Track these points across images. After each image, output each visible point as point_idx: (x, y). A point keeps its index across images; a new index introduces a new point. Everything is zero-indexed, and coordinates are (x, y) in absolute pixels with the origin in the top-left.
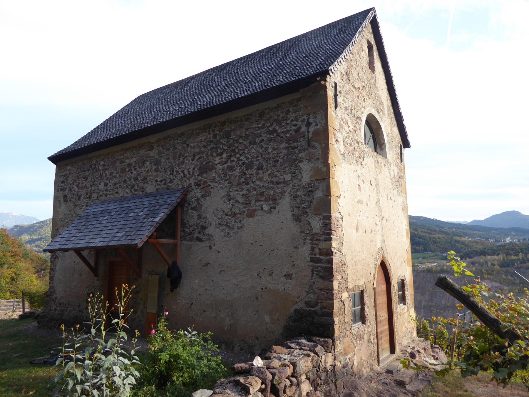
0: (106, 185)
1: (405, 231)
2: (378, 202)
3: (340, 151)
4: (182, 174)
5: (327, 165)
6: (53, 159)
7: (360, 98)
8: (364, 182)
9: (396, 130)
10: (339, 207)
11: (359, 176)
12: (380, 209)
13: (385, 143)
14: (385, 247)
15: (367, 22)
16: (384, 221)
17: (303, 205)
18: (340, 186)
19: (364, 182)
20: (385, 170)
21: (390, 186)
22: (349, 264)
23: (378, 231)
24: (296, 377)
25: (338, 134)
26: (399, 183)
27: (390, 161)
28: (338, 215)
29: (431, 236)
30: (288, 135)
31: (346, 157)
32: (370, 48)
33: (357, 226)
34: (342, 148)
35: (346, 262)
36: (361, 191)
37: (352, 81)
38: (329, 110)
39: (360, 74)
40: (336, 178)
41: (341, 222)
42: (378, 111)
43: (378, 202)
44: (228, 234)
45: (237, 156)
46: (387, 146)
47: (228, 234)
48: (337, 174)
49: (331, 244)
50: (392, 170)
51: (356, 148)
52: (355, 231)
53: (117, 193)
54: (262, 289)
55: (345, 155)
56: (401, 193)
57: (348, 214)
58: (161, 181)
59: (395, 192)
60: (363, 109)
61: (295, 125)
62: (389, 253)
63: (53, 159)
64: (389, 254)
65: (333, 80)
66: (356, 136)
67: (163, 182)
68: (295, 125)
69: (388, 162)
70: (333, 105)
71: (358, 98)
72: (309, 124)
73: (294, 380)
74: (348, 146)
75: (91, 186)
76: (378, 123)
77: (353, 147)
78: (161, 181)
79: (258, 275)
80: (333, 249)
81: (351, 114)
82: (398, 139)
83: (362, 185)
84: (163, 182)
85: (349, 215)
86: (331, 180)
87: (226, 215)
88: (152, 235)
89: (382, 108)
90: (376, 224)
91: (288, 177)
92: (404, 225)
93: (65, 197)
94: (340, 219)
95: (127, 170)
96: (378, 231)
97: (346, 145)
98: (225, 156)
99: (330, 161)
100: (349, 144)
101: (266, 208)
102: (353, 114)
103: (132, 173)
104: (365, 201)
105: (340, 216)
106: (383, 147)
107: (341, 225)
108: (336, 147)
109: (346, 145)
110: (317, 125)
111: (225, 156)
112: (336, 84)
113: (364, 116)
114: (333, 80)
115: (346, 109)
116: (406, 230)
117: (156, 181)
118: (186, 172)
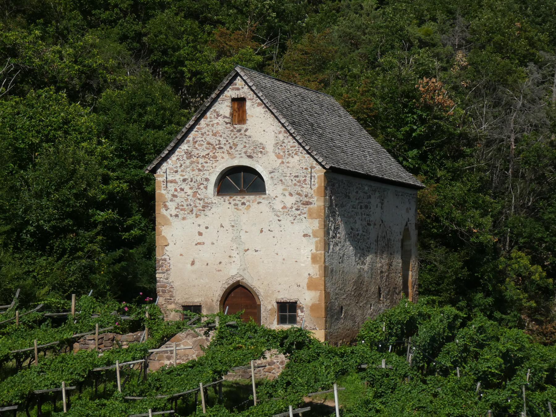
3: (171, 215)
10: (167, 252)
25: (169, 204)
40: (163, 234)
52: (189, 265)
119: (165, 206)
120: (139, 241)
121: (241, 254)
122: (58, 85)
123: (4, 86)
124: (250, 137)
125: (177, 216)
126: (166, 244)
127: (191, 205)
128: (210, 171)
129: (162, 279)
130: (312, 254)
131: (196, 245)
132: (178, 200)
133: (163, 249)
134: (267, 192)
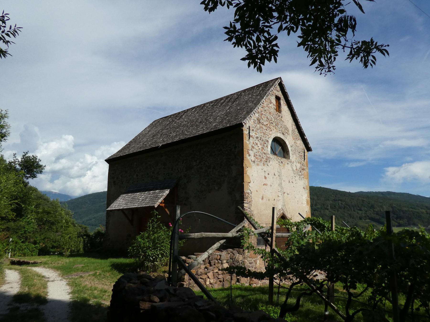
0: (137, 175)
1: (306, 201)
2: (280, 185)
3: (252, 160)
4: (177, 171)
5: (243, 168)
6: (108, 161)
7: (268, 130)
8: (268, 174)
9: (300, 142)
10: (250, 188)
11: (265, 171)
12: (282, 188)
13: (289, 151)
14: (285, 209)
15: (277, 83)
16: (286, 194)
17: (232, 187)
18: (250, 177)
19: (268, 174)
20: (288, 167)
21: (293, 175)
22: (256, 215)
23: (280, 200)
24: (221, 261)
25: (250, 152)
26: (301, 173)
27: (293, 161)
28: (249, 191)
29: (414, 210)
30: (227, 152)
31: (256, 162)
32: (278, 99)
33: (263, 197)
34: (253, 158)
35: (253, 214)
36: (266, 179)
37: (262, 122)
38: (245, 141)
39: (268, 117)
40: (248, 174)
41: (251, 195)
42: (283, 134)
43: (280, 185)
44: (199, 201)
45: (204, 162)
46: (291, 153)
47: (199, 201)
48: (248, 171)
49: (244, 205)
50: (294, 166)
51: (264, 157)
52: (261, 199)
53: (143, 180)
54: (214, 228)
55: (255, 162)
56: (303, 178)
57: (256, 191)
58: (167, 174)
59: (297, 178)
60: (270, 136)
61: (230, 147)
62: (289, 212)
63: (108, 161)
64: (288, 213)
65: (248, 125)
66: (264, 150)
67: (168, 175)
68: (230, 147)
69: (291, 162)
70: (248, 138)
71: (267, 130)
72: (235, 147)
73: (220, 261)
74: (258, 157)
75: (129, 176)
76: (283, 140)
77: (262, 157)
78: (167, 174)
79: (212, 221)
80: (245, 207)
81: (260, 140)
82: (302, 146)
83: (267, 176)
84: (168, 175)
85: (257, 191)
86: (245, 175)
87: (198, 192)
88: (162, 202)
89: (287, 131)
90: (278, 196)
91: (226, 173)
92: (305, 197)
93: (114, 182)
94: (250, 193)
95: (149, 167)
96: (280, 200)
97: (256, 156)
98: (198, 161)
99: (244, 165)
100: (258, 156)
101: (216, 188)
102: (262, 139)
103: (151, 169)
104: (269, 184)
105: (250, 192)
106: (288, 153)
107: (251, 196)
108: (249, 158)
109: (256, 156)
110: (239, 148)
111: (198, 161)
112: (249, 127)
113: (270, 139)
114: (248, 125)
115: (257, 138)
116: (307, 200)
117: (164, 174)
118: (179, 169)
119: (248, 153)
120: (315, 210)
121: (282, 195)
122: (253, 48)
123: (265, 24)
124: (283, 122)
125: (254, 162)
126: (249, 181)
127: (261, 156)
128: (269, 136)
129: (247, 208)
130: (307, 199)
131: (264, 185)
132: (255, 150)
133: (248, 185)
134: (290, 158)
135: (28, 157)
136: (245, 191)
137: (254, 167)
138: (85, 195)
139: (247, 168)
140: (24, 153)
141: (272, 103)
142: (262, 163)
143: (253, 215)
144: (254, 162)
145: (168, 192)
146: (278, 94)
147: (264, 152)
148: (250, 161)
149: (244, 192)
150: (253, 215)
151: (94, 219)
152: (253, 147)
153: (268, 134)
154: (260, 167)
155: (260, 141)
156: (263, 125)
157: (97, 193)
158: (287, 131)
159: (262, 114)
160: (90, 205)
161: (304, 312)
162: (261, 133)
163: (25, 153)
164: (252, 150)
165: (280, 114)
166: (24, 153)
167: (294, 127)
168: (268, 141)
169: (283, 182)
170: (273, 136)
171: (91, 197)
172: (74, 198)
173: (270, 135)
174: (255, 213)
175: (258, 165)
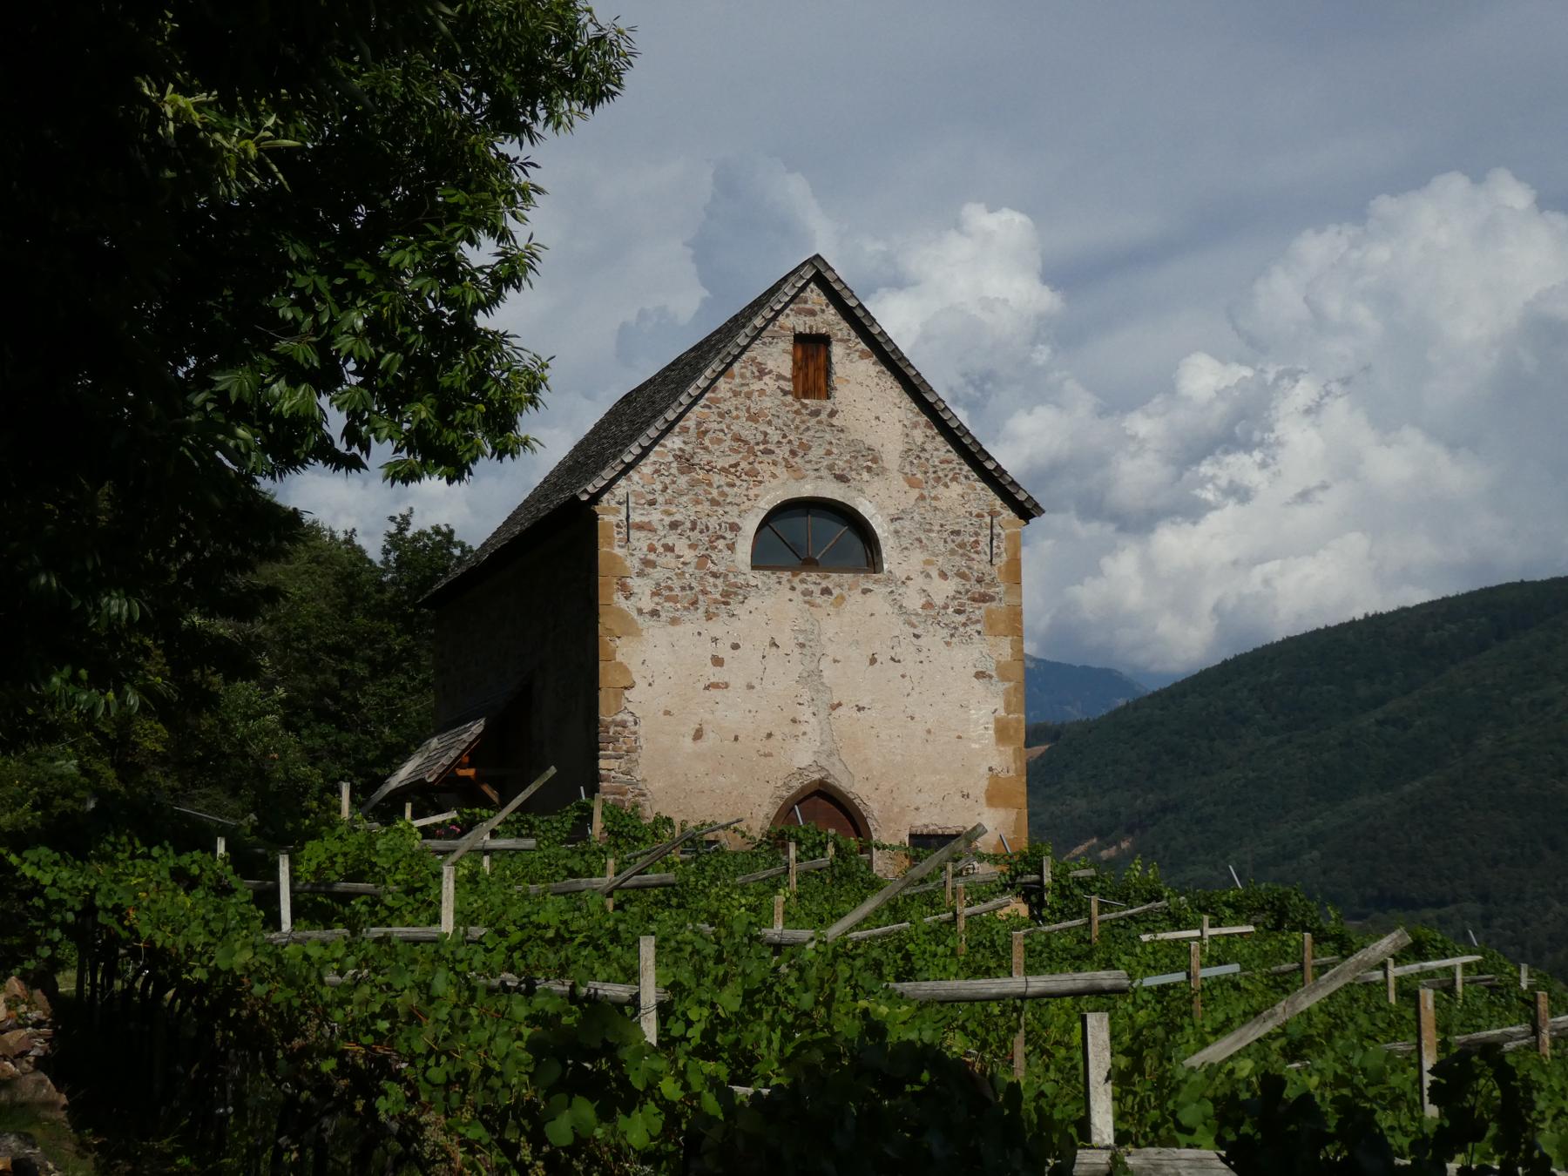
3: (640, 612)
10: (628, 705)
25: (634, 583)
40: (619, 658)
69: (890, 580)
104: (737, 682)
105: (631, 719)
119: (624, 587)
121: (822, 715)
124: (842, 431)
125: (654, 613)
127: (691, 588)
128: (743, 507)
130: (997, 721)
131: (707, 688)
132: (657, 574)
135: (415, 539)
136: (604, 716)
137: (654, 632)
138: (1225, 663)
139: (618, 641)
140: (392, 519)
141: (770, 372)
142: (702, 610)
143: (644, 795)
144: (654, 613)
145: (481, 729)
146: (811, 328)
147: (714, 569)
148: (634, 614)
149: (597, 720)
150: (644, 795)
151: (1315, 853)
152: (647, 563)
153: (737, 500)
154: (687, 629)
155: (688, 533)
156: (708, 471)
157: (1317, 633)
158: (869, 464)
159: (705, 432)
160: (1273, 740)
161: (737, 1102)
162: (697, 502)
163: (399, 519)
164: (640, 574)
165: (828, 405)
166: (392, 519)
167: (923, 432)
168: (734, 528)
169: (825, 664)
170: (767, 503)
171: (1276, 675)
172: (1155, 687)
173: (747, 503)
174: (655, 786)
175: (674, 621)
